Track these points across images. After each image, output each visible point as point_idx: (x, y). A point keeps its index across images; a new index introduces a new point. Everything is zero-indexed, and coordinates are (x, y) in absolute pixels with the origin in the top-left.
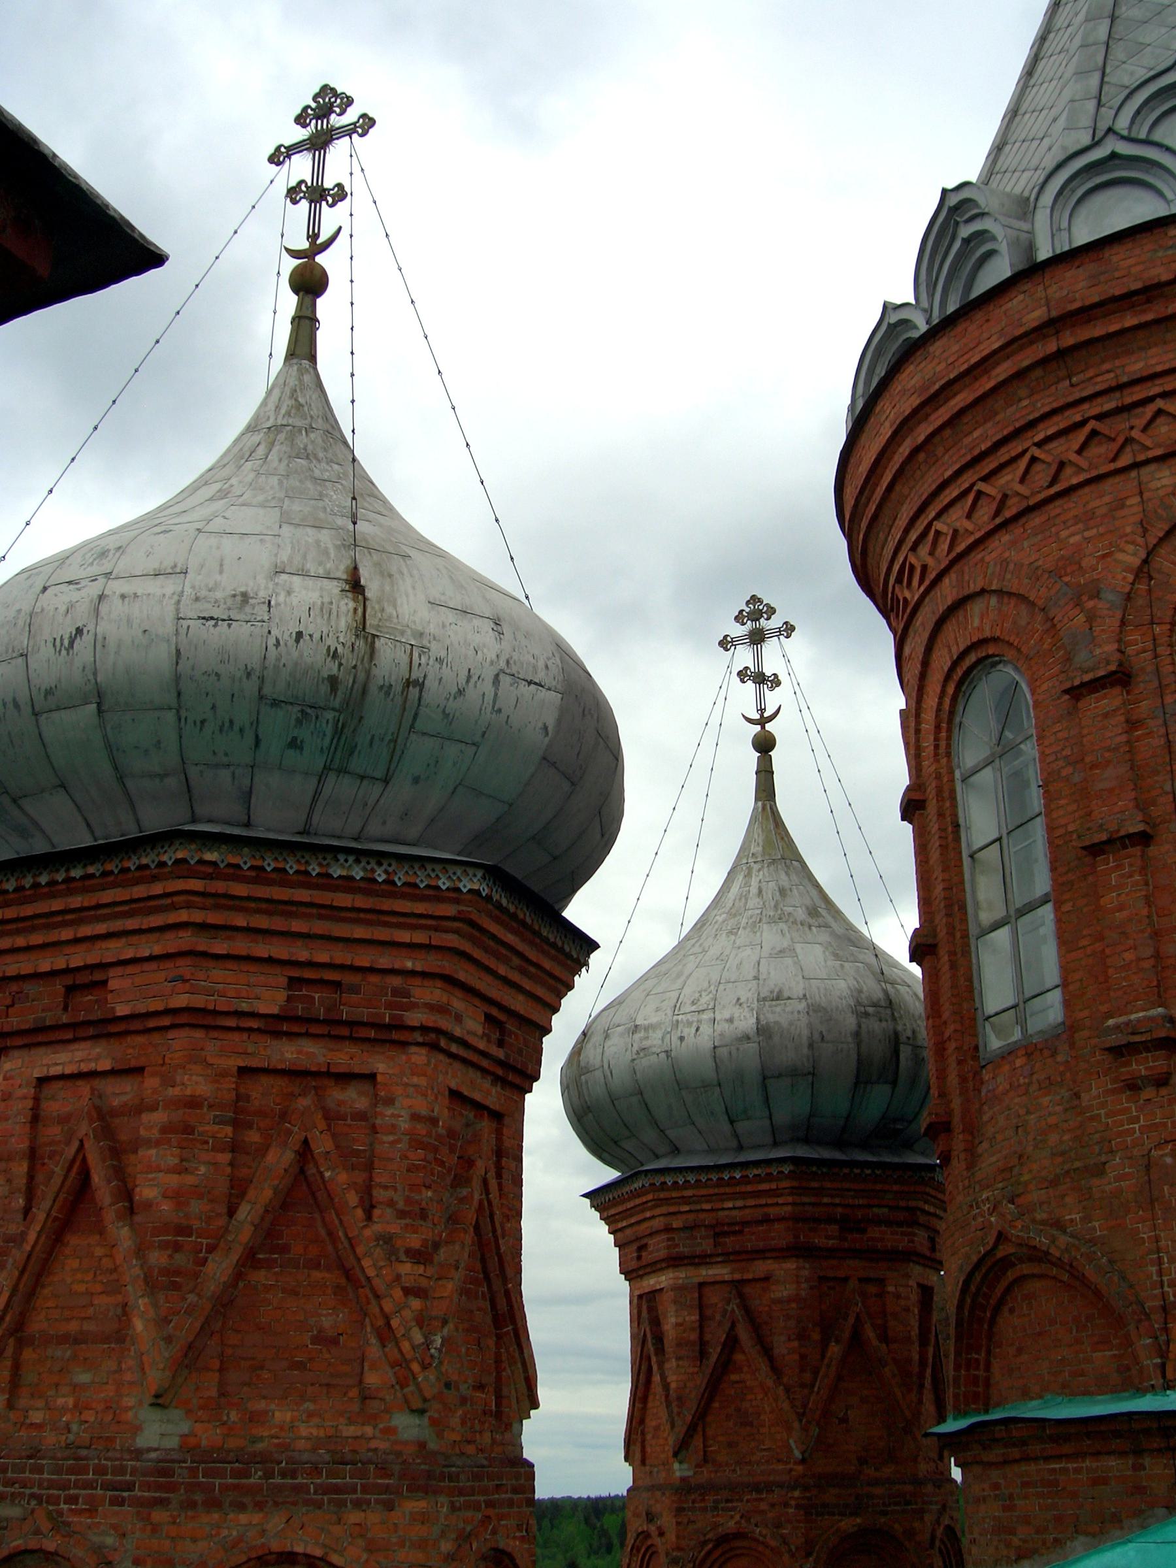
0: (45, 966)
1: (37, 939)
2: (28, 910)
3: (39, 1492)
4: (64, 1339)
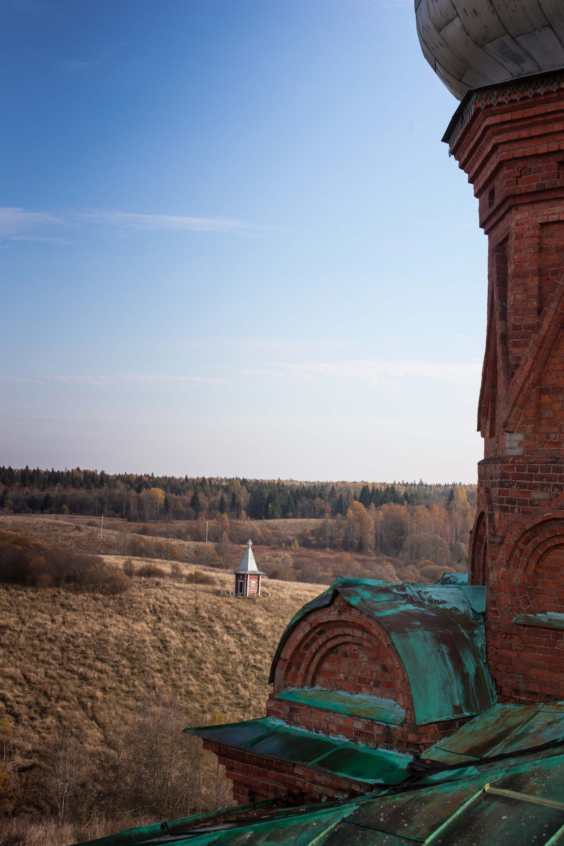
0: (543, 149)
1: (536, 131)
2: (531, 112)
3: (560, 483)
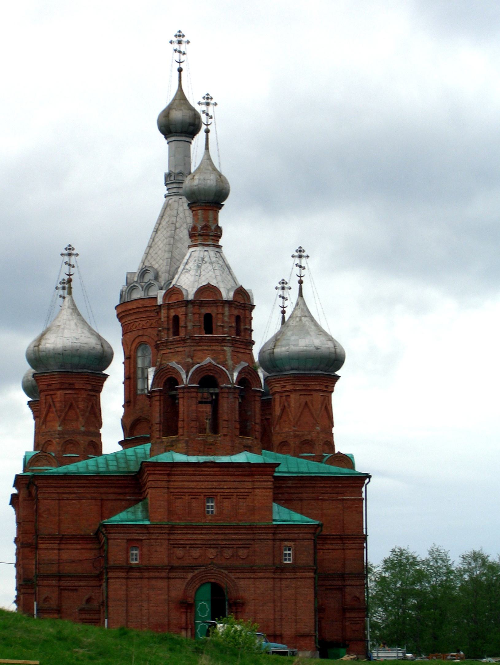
4: (69, 420)
